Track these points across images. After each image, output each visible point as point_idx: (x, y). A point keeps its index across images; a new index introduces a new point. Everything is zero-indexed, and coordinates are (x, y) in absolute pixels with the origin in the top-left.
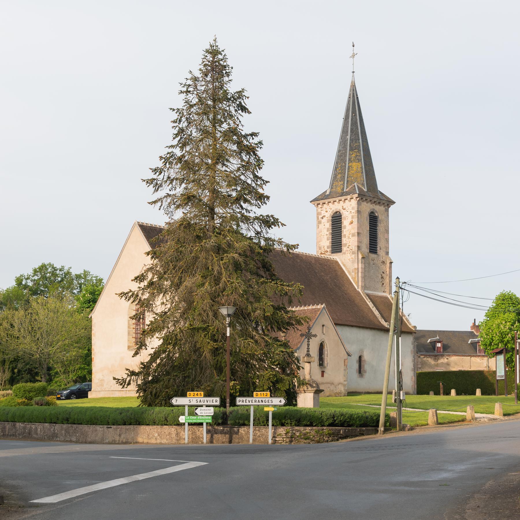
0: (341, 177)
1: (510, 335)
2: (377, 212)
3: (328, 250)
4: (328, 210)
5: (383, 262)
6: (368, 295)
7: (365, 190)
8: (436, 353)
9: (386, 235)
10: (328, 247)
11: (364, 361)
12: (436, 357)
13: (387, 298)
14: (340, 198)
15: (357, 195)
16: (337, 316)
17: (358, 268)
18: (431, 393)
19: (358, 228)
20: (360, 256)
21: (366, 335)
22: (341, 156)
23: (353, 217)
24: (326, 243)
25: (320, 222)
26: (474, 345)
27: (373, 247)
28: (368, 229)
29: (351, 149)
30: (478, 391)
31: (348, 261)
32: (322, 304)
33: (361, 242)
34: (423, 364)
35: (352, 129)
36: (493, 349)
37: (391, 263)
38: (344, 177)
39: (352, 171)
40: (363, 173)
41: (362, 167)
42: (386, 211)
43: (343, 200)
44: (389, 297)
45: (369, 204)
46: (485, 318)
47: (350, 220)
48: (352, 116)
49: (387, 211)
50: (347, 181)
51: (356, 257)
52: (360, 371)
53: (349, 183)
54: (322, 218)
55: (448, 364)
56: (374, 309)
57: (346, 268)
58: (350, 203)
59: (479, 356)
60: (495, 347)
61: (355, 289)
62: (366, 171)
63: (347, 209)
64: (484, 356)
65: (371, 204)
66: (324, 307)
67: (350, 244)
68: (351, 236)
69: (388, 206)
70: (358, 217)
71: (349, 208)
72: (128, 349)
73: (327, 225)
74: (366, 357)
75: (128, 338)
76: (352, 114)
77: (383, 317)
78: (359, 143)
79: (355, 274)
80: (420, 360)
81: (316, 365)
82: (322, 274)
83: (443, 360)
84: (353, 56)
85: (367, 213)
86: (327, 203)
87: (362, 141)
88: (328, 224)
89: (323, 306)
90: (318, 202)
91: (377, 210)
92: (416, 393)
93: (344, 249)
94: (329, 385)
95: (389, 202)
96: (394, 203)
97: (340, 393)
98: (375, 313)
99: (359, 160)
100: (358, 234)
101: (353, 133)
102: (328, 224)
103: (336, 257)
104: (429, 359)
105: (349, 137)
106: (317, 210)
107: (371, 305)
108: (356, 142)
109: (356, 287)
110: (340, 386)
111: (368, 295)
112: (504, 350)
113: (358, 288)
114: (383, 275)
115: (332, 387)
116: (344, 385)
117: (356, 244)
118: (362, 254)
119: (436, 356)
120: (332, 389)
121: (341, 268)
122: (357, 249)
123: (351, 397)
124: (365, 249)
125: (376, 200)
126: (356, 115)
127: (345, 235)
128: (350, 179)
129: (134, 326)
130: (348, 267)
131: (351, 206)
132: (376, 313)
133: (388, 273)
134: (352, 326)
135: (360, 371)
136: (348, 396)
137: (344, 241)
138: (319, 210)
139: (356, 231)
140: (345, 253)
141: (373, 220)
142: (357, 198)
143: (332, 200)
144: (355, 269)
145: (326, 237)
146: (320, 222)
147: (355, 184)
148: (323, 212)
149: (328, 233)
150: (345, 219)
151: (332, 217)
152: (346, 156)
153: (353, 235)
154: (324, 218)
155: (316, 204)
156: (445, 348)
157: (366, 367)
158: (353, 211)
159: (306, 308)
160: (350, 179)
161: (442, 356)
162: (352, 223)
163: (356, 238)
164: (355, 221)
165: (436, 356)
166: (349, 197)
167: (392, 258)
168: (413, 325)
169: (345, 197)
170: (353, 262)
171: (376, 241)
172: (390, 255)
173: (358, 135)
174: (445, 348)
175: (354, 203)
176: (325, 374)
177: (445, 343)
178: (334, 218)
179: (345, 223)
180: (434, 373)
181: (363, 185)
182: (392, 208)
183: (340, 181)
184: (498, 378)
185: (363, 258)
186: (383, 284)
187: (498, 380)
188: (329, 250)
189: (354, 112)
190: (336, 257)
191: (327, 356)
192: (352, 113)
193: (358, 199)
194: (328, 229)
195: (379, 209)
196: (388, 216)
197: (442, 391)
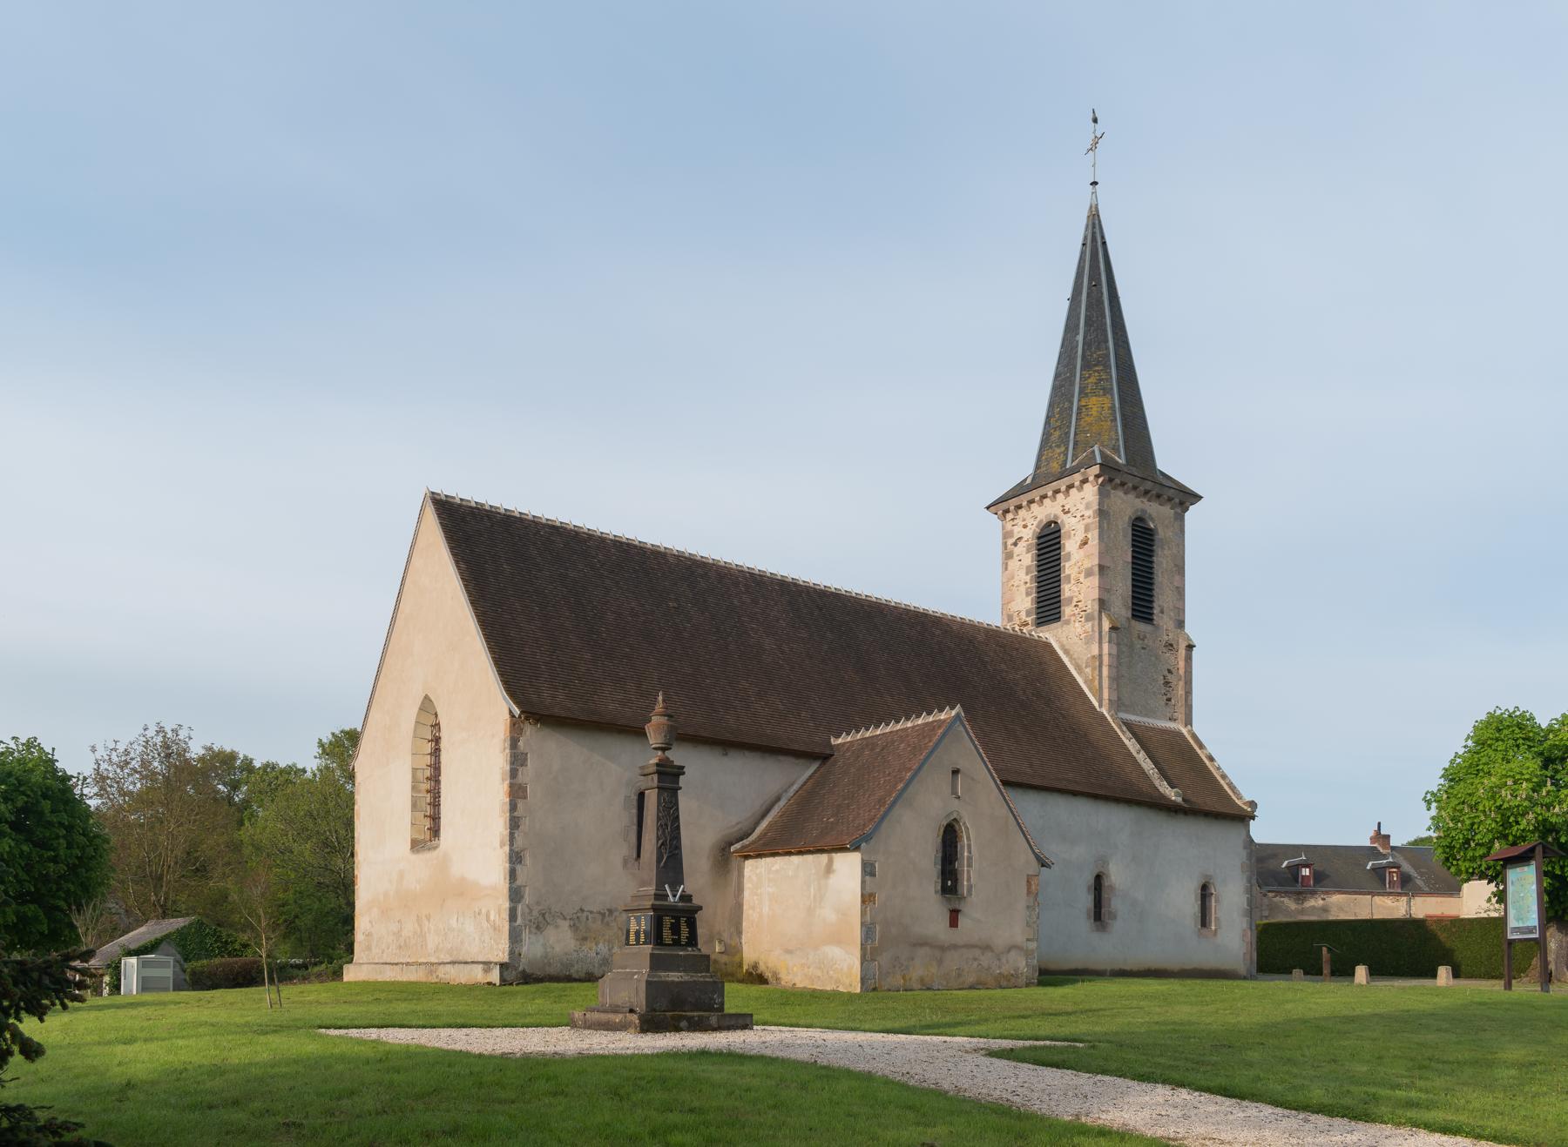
1: (1531, 816)
3: (1029, 620)
4: (1029, 522)
6: (1130, 726)
7: (1122, 461)
8: (1299, 888)
9: (1177, 578)
10: (1028, 613)
11: (1111, 887)
12: (1300, 896)
13: (1180, 734)
15: (1096, 470)
16: (1031, 766)
17: (1100, 655)
18: (1297, 972)
20: (1106, 625)
21: (1116, 821)
23: (1087, 529)
24: (1024, 603)
26: (1379, 873)
27: (1143, 603)
28: (1129, 559)
29: (1086, 365)
32: (952, 708)
33: (1108, 591)
34: (1273, 908)
36: (1473, 859)
37: (1190, 647)
38: (1067, 434)
41: (1112, 408)
43: (1063, 488)
44: (1184, 731)
45: (1131, 497)
46: (1442, 781)
47: (1080, 536)
49: (1181, 519)
50: (1076, 443)
52: (1099, 913)
54: (1015, 544)
55: (1325, 910)
56: (1142, 758)
58: (1082, 494)
59: (1390, 894)
60: (1481, 851)
62: (1123, 416)
64: (1400, 894)
66: (958, 715)
70: (1101, 527)
71: (1077, 508)
72: (412, 847)
73: (1025, 558)
74: (1117, 876)
77: (1164, 775)
80: (1266, 901)
81: (932, 890)
82: (1003, 666)
83: (1315, 902)
87: (1115, 344)
89: (954, 713)
90: (1004, 506)
92: (1254, 971)
93: (1067, 611)
94: (977, 952)
95: (1185, 498)
97: (1015, 976)
98: (1144, 765)
99: (1107, 391)
100: (1102, 568)
103: (1049, 634)
104: (1286, 900)
105: (1080, 338)
107: (1132, 745)
108: (1098, 348)
109: (1096, 704)
110: (1013, 953)
111: (1130, 726)
112: (1539, 850)
114: (1169, 677)
115: (986, 959)
116: (1028, 954)
117: (1095, 594)
118: (1111, 621)
119: (1300, 893)
120: (985, 964)
121: (1059, 659)
122: (1097, 607)
123: (1050, 990)
125: (1148, 485)
126: (1098, 285)
128: (1081, 437)
132: (1147, 765)
133: (1182, 672)
134: (1075, 794)
135: (1099, 913)
136: (1041, 983)
137: (1067, 590)
138: (1009, 526)
139: (1096, 562)
140: (1068, 622)
141: (1143, 541)
142: (1097, 476)
145: (1023, 589)
146: (1008, 556)
147: (1096, 448)
152: (1072, 384)
153: (1089, 573)
156: (1319, 877)
157: (1116, 904)
158: (1089, 513)
159: (909, 724)
160: (1081, 437)
161: (1313, 893)
162: (1085, 543)
163: (1095, 581)
164: (1093, 536)
165: (1300, 893)
166: (1077, 478)
168: (1248, 798)
170: (1088, 641)
172: (1188, 629)
174: (1319, 877)
175: (1090, 492)
176: (962, 920)
177: (1316, 867)
179: (1070, 546)
180: (1298, 924)
181: (1116, 449)
182: (1193, 515)
184: (1510, 937)
185: (1113, 628)
187: (1511, 942)
190: (1049, 634)
191: (969, 865)
192: (1090, 280)
195: (1158, 513)
197: (1326, 970)
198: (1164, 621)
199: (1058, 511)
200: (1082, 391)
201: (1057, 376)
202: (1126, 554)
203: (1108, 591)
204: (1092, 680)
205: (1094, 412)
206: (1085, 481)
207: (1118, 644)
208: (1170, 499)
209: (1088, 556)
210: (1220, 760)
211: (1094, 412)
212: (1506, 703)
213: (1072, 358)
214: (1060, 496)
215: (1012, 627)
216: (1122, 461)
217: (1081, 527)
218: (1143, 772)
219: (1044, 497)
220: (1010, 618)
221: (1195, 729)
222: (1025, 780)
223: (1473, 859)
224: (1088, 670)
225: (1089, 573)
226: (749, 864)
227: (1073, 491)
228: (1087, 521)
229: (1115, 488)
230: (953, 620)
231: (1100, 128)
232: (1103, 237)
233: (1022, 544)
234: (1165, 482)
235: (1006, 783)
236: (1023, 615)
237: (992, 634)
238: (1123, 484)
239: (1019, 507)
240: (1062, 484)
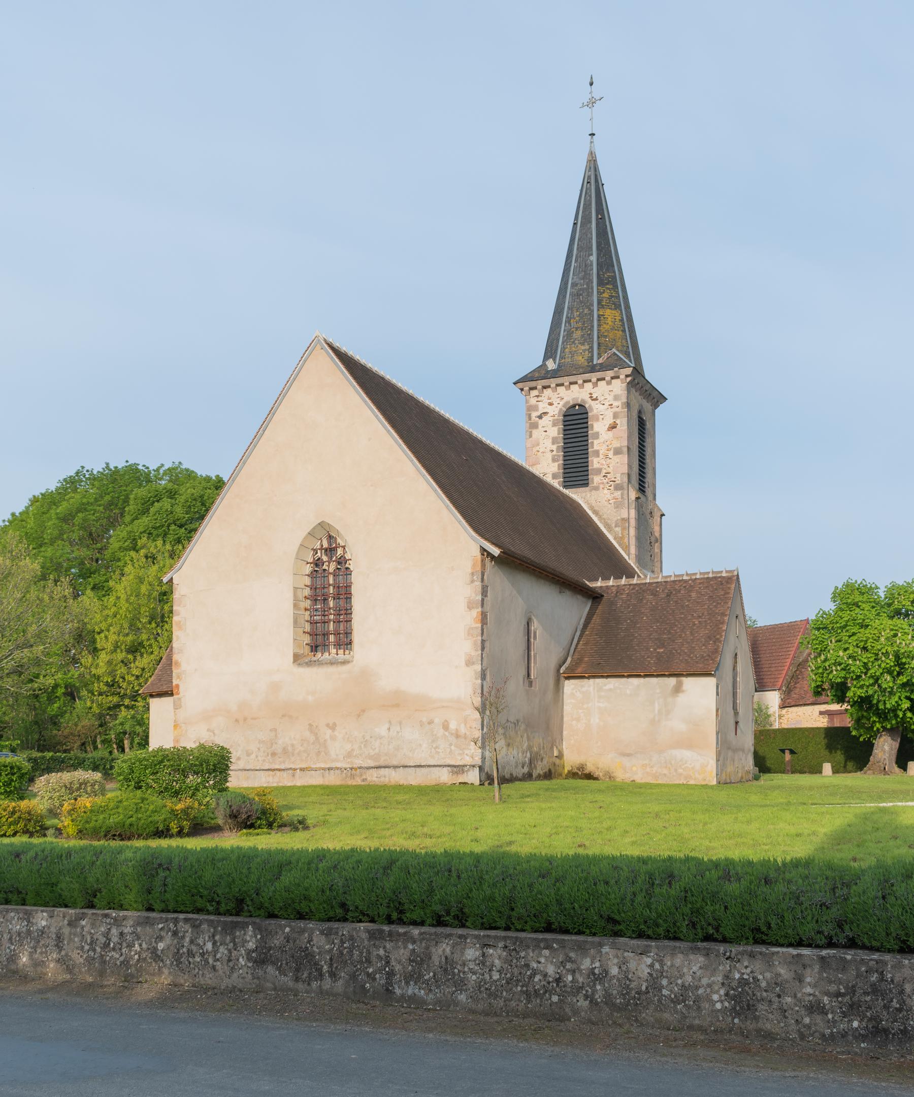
0: (583, 336)
4: (555, 401)
14: (587, 376)
22: (578, 295)
23: (615, 416)
25: (535, 426)
29: (601, 283)
30: (827, 768)
38: (590, 336)
39: (605, 326)
41: (622, 320)
43: (594, 380)
47: (609, 421)
48: (597, 219)
50: (599, 344)
51: (625, 497)
53: (602, 348)
54: (540, 417)
57: (600, 518)
63: (601, 398)
67: (610, 470)
68: (611, 454)
69: (656, 406)
72: (294, 661)
75: (295, 633)
76: (597, 216)
78: (614, 272)
84: (592, 103)
86: (553, 385)
88: (556, 429)
90: (533, 384)
93: (596, 479)
102: (556, 429)
103: (576, 495)
105: (594, 258)
106: (527, 402)
108: (608, 270)
109: (626, 557)
122: (626, 479)
129: (308, 603)
131: (612, 394)
137: (595, 463)
138: (533, 401)
140: (596, 488)
142: (627, 376)
143: (566, 380)
144: (623, 519)
145: (549, 456)
148: (541, 405)
149: (554, 447)
150: (597, 420)
151: (565, 416)
152: (590, 294)
153: (617, 452)
154: (545, 418)
162: (613, 427)
166: (609, 374)
169: (599, 375)
170: (618, 506)
179: (599, 427)
183: (583, 344)
190: (576, 495)
193: (629, 379)
199: (586, 397)
200: (599, 302)
205: (609, 321)
211: (609, 321)
212: (857, 578)
217: (609, 414)
223: (862, 687)
224: (618, 529)
225: (617, 452)
226: (567, 682)
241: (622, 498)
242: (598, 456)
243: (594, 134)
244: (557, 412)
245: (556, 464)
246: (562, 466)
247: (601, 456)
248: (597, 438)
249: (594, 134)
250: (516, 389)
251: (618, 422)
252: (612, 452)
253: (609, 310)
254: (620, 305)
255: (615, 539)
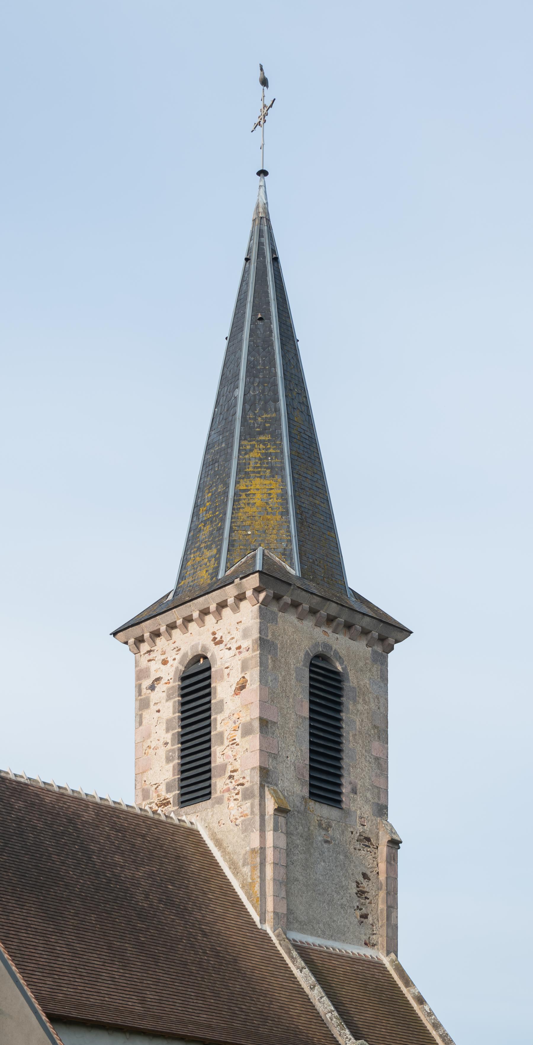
0: (211, 533)
2: (340, 659)
4: (171, 655)
5: (366, 840)
6: (304, 952)
7: (295, 571)
9: (376, 744)
13: (379, 966)
15: (254, 581)
16: (143, 1001)
17: (263, 849)
19: (262, 703)
20: (271, 806)
23: (244, 667)
24: (165, 772)
27: (326, 777)
28: (306, 714)
29: (248, 433)
31: (231, 826)
33: (275, 757)
35: (251, 366)
37: (395, 843)
38: (220, 530)
39: (247, 509)
40: (286, 513)
41: (283, 495)
42: (375, 661)
43: (213, 607)
44: (386, 961)
45: (308, 624)
47: (235, 678)
49: (381, 661)
50: (231, 544)
51: (257, 810)
58: (238, 616)
61: (253, 924)
62: (299, 508)
63: (226, 639)
65: (318, 625)
67: (237, 765)
70: (263, 664)
71: (231, 636)
76: (254, 314)
78: (277, 410)
79: (253, 868)
82: (118, 858)
85: (302, 655)
90: (136, 631)
91: (343, 653)
93: (219, 784)
95: (386, 632)
96: (405, 632)
99: (276, 471)
100: (264, 723)
101: (255, 376)
102: (170, 704)
103: (197, 818)
105: (240, 393)
107: (304, 977)
108: (265, 409)
109: (256, 918)
111: (304, 952)
113: (263, 921)
117: (255, 760)
121: (207, 854)
122: (257, 779)
124: (295, 784)
125: (333, 609)
127: (221, 735)
128: (235, 536)
130: (230, 849)
131: (241, 627)
132: (324, 1006)
133: (382, 877)
137: (220, 754)
139: (256, 713)
140: (220, 801)
141: (326, 688)
142: (257, 591)
144: (253, 851)
145: (162, 752)
146: (143, 704)
149: (168, 737)
152: (228, 460)
153: (247, 731)
155: (131, 641)
158: (247, 643)
160: (235, 536)
162: (242, 687)
163: (254, 741)
166: (230, 592)
167: (397, 828)
171: (339, 759)
172: (393, 817)
173: (275, 385)
175: (249, 613)
178: (188, 682)
179: (222, 690)
181: (286, 554)
182: (399, 656)
183: (209, 548)
185: (280, 810)
186: (365, 916)
188: (172, 796)
189: (261, 318)
190: (197, 818)
193: (262, 596)
194: (169, 722)
196: (384, 678)
198: (357, 804)
199: (207, 640)
201: (209, 447)
202: (299, 706)
203: (275, 757)
204: (252, 884)
205: (258, 500)
206: (241, 597)
207: (288, 834)
208: (365, 632)
209: (246, 706)
210: (434, 1003)
211: (258, 500)
213: (230, 422)
214: (210, 619)
215: (148, 806)
216: (295, 571)
217: (236, 664)
218: (317, 1015)
219: (188, 620)
220: (146, 795)
221: (403, 959)
222: (129, 1022)
227: (226, 612)
228: (245, 655)
229: (284, 609)
230: (47, 789)
231: (270, 93)
232: (274, 251)
233: (160, 687)
234: (357, 606)
235: (55, 1019)
236: (163, 788)
237: (109, 816)
238: (295, 605)
239: (156, 634)
240: (211, 601)
241: (252, 812)
242: (222, 743)
243: (259, 173)
244: (172, 675)
245: (171, 765)
246: (178, 768)
247: (226, 742)
248: (221, 710)
249: (259, 173)
250: (116, 643)
251: (247, 677)
252: (239, 733)
253: (258, 481)
254: (283, 468)
255: (243, 887)
